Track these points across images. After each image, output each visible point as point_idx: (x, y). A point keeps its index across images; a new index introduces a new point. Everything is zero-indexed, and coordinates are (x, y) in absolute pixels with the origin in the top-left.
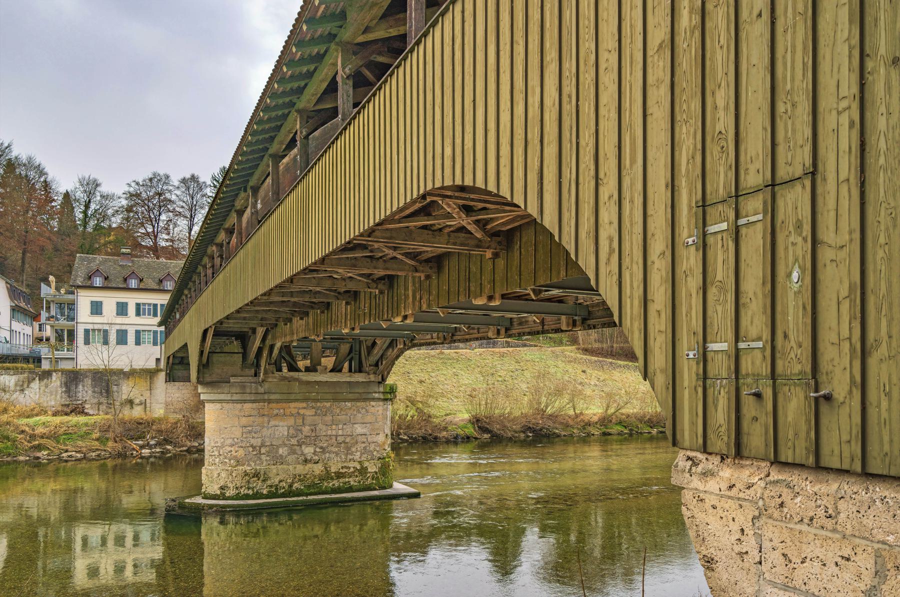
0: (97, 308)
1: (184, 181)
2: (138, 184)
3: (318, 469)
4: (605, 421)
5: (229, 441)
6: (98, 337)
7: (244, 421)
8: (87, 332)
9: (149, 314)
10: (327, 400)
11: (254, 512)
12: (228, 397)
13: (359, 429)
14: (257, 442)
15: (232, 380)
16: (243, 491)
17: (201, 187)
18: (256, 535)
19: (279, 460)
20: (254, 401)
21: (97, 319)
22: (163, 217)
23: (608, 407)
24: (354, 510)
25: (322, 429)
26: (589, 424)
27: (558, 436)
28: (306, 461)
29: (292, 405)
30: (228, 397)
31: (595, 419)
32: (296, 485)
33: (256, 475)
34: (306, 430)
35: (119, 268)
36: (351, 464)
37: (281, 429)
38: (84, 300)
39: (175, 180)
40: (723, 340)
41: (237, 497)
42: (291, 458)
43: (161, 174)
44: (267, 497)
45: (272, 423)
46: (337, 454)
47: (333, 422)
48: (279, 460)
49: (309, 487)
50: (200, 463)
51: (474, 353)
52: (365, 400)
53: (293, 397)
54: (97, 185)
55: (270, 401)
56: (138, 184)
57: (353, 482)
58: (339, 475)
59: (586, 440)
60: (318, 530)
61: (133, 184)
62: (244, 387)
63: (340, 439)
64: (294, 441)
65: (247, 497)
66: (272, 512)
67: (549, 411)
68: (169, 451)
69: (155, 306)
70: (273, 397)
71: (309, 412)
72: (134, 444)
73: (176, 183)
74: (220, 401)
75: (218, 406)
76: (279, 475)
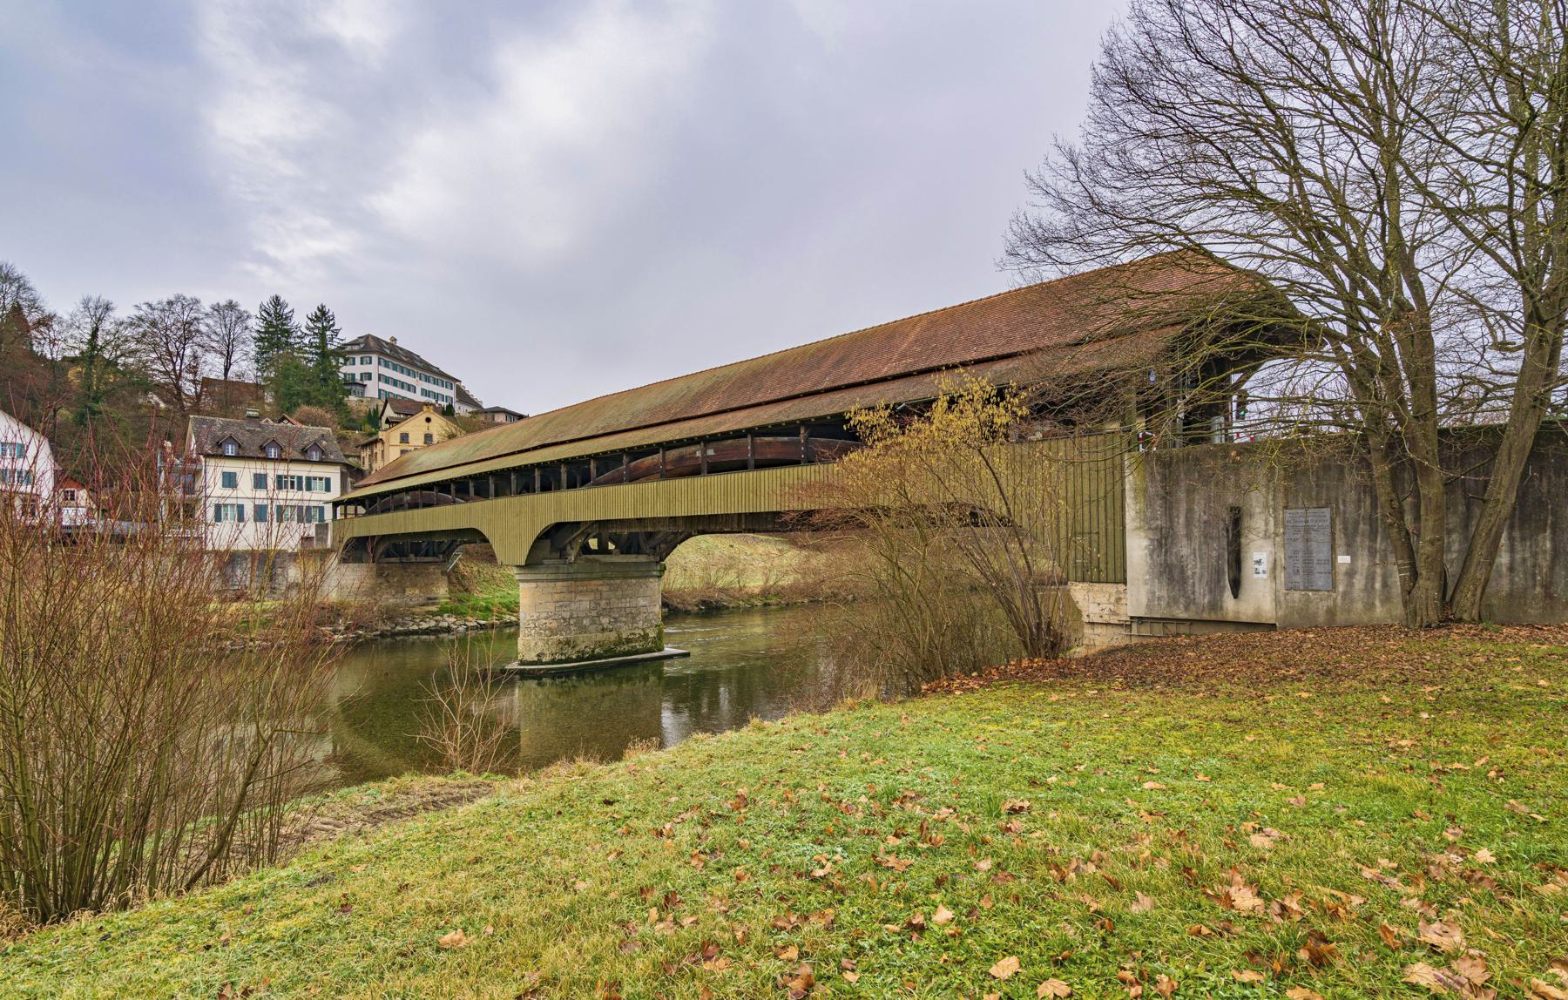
0: (230, 481)
1: (217, 308)
2: (150, 306)
3: (613, 636)
4: (765, 593)
5: (544, 615)
6: (231, 513)
7: (556, 597)
8: (218, 508)
9: (292, 487)
10: (618, 578)
11: (566, 673)
12: (544, 577)
13: (642, 602)
14: (567, 615)
15: (546, 562)
16: (558, 657)
17: (242, 317)
18: (568, 693)
19: (583, 629)
20: (563, 580)
21: (228, 492)
22: (188, 352)
23: (767, 581)
24: (639, 671)
25: (615, 603)
26: (752, 596)
27: (728, 608)
28: (603, 630)
29: (593, 582)
30: (544, 577)
31: (757, 591)
32: (597, 650)
33: (568, 642)
34: (603, 602)
35: (248, 435)
36: (637, 631)
37: (584, 604)
38: (214, 471)
39: (206, 306)
40: (1111, 577)
41: (553, 662)
42: (592, 628)
43: (188, 297)
44: (576, 661)
45: (578, 598)
46: (625, 623)
47: (624, 597)
48: (583, 629)
49: (606, 651)
50: (515, 636)
51: (707, 537)
52: (646, 577)
53: (594, 576)
54: (107, 308)
55: (576, 580)
56: (150, 306)
57: (638, 645)
58: (628, 641)
59: (749, 611)
60: (614, 688)
61: (145, 307)
62: (558, 568)
63: (628, 610)
64: (594, 613)
65: (560, 661)
66: (581, 673)
67: (720, 584)
68: (359, 636)
69: (300, 478)
70: (579, 576)
71: (605, 589)
72: (327, 629)
73: (209, 310)
74: (536, 581)
75: (534, 585)
76: (586, 642)
